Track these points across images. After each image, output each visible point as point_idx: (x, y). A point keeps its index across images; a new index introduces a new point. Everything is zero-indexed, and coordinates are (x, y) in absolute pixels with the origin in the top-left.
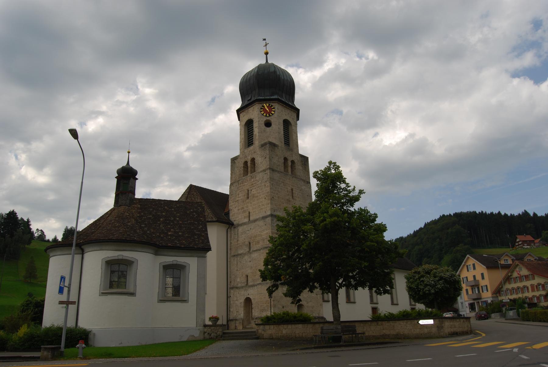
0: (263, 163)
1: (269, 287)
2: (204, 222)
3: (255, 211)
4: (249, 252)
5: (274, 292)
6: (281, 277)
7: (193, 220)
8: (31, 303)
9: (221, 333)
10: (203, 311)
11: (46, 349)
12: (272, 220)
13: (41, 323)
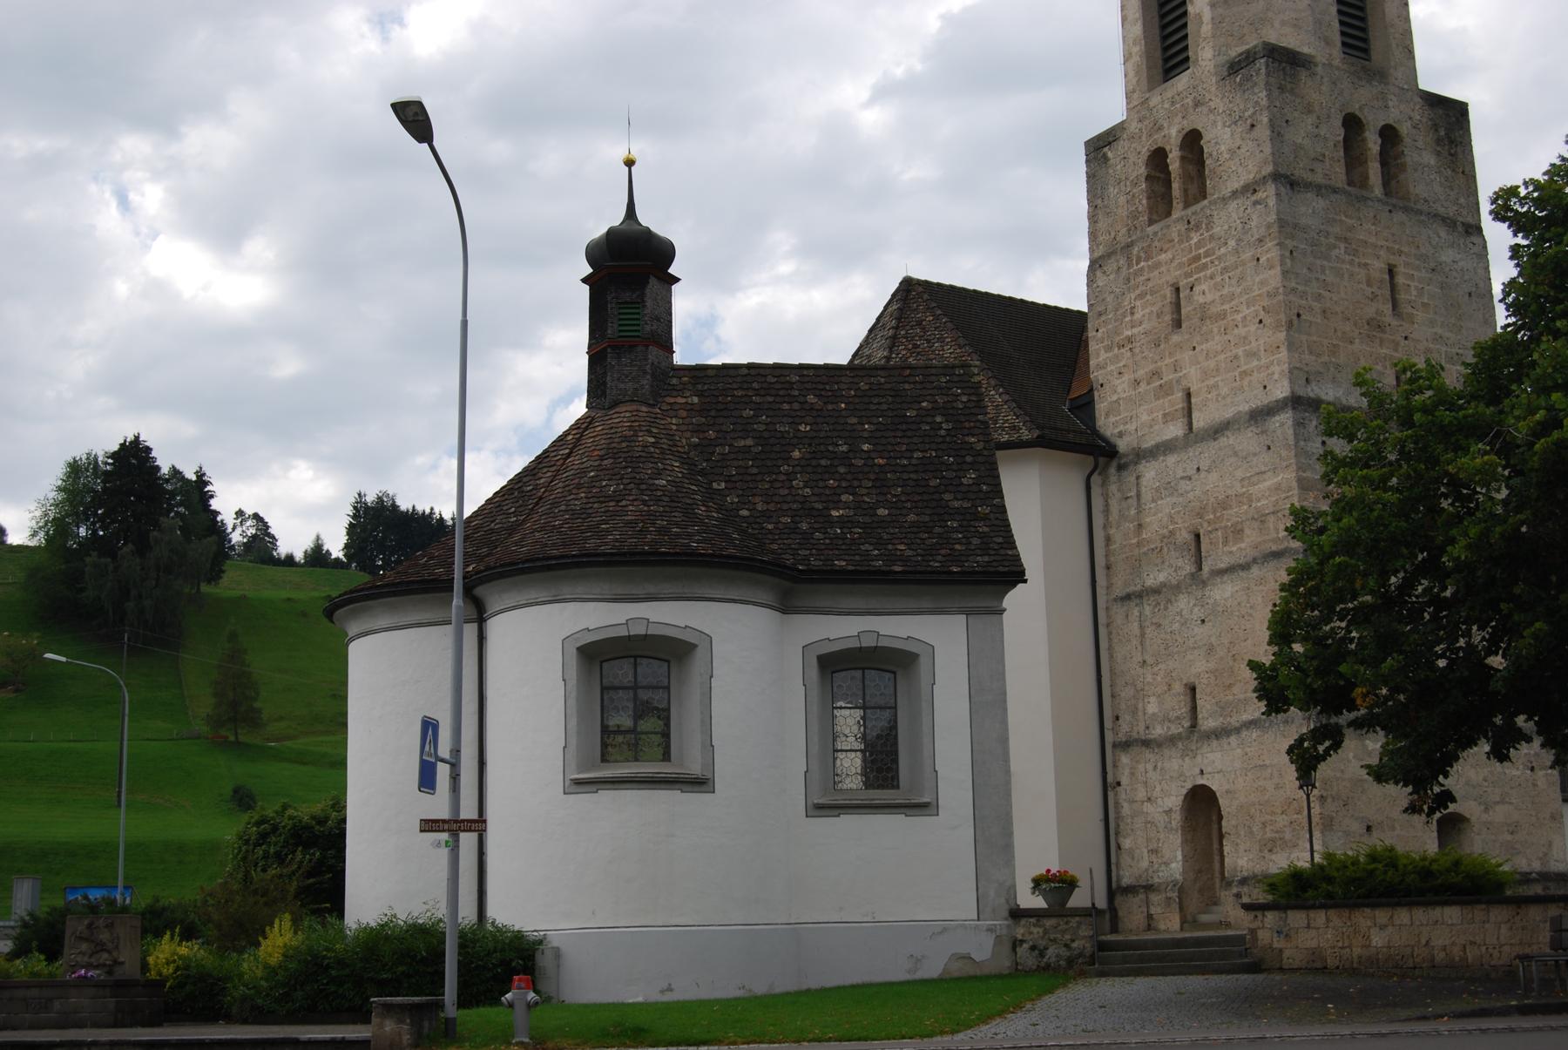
0: (1242, 150)
1: (1301, 740)
2: (986, 453)
3: (1216, 386)
4: (1198, 578)
5: (1324, 759)
6: (1352, 691)
7: (934, 446)
8: (275, 829)
9: (1088, 945)
10: (1007, 849)
11: (388, 1008)
12: (1299, 424)
13: (338, 908)
